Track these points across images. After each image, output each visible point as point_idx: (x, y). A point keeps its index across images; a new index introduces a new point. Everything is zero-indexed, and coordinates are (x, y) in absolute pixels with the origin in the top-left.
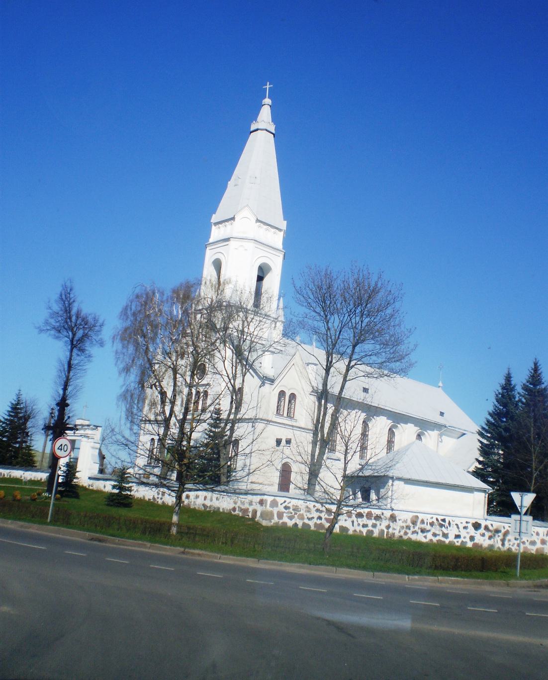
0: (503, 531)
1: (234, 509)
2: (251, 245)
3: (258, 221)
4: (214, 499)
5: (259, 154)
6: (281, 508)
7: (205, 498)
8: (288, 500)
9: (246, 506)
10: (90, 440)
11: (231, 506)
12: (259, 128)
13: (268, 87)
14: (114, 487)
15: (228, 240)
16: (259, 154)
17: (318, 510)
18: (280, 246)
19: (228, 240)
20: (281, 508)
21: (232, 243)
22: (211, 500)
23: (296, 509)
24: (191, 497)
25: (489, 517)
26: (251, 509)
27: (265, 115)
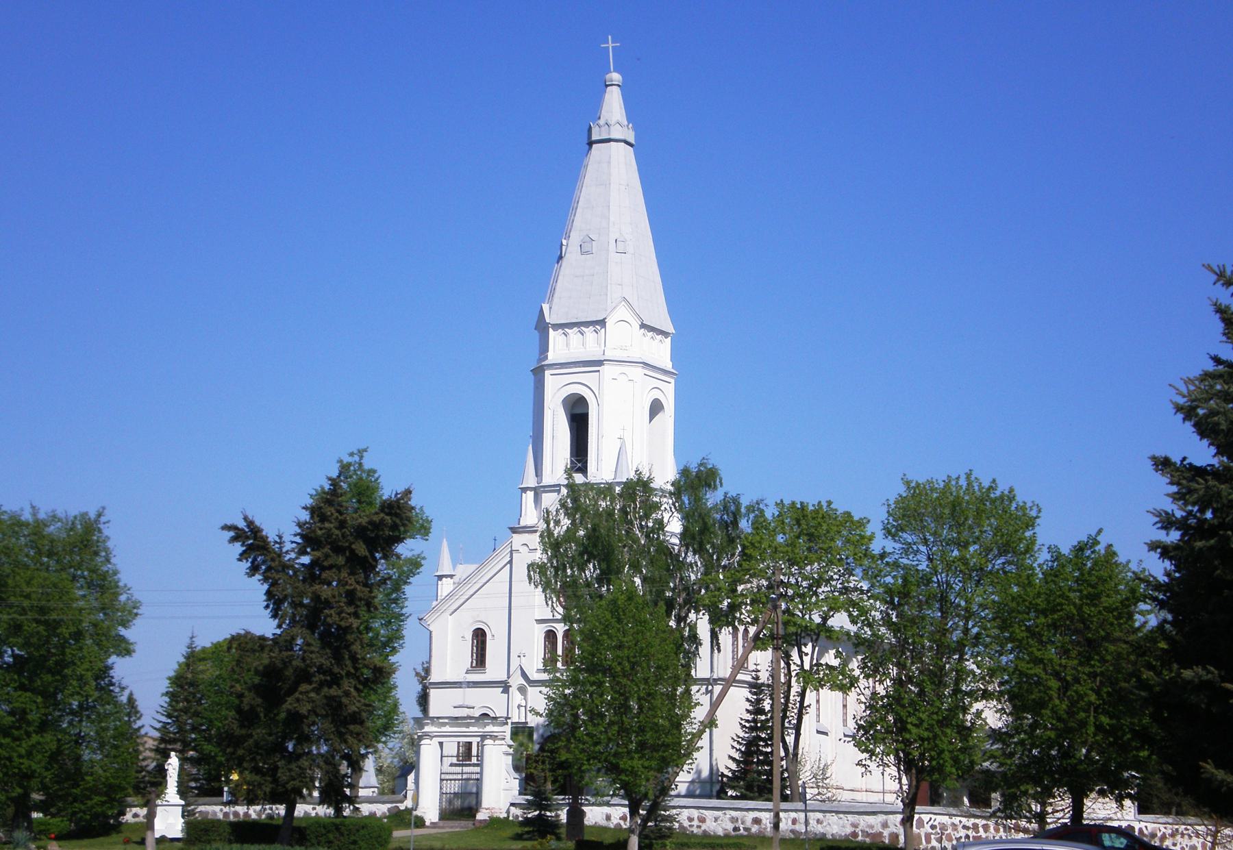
0: (1159, 834)
1: (855, 834)
2: (639, 371)
3: (643, 326)
4: (812, 822)
5: (613, 191)
6: (927, 828)
7: (794, 821)
8: (933, 817)
9: (878, 828)
10: (497, 742)
11: (849, 830)
12: (612, 137)
13: (611, 45)
14: (624, 818)
15: (599, 363)
16: (613, 191)
17: (965, 827)
18: (668, 366)
19: (599, 363)
20: (927, 828)
21: (606, 369)
22: (807, 823)
23: (943, 827)
24: (764, 821)
25: (1142, 817)
26: (886, 833)
27: (614, 106)
